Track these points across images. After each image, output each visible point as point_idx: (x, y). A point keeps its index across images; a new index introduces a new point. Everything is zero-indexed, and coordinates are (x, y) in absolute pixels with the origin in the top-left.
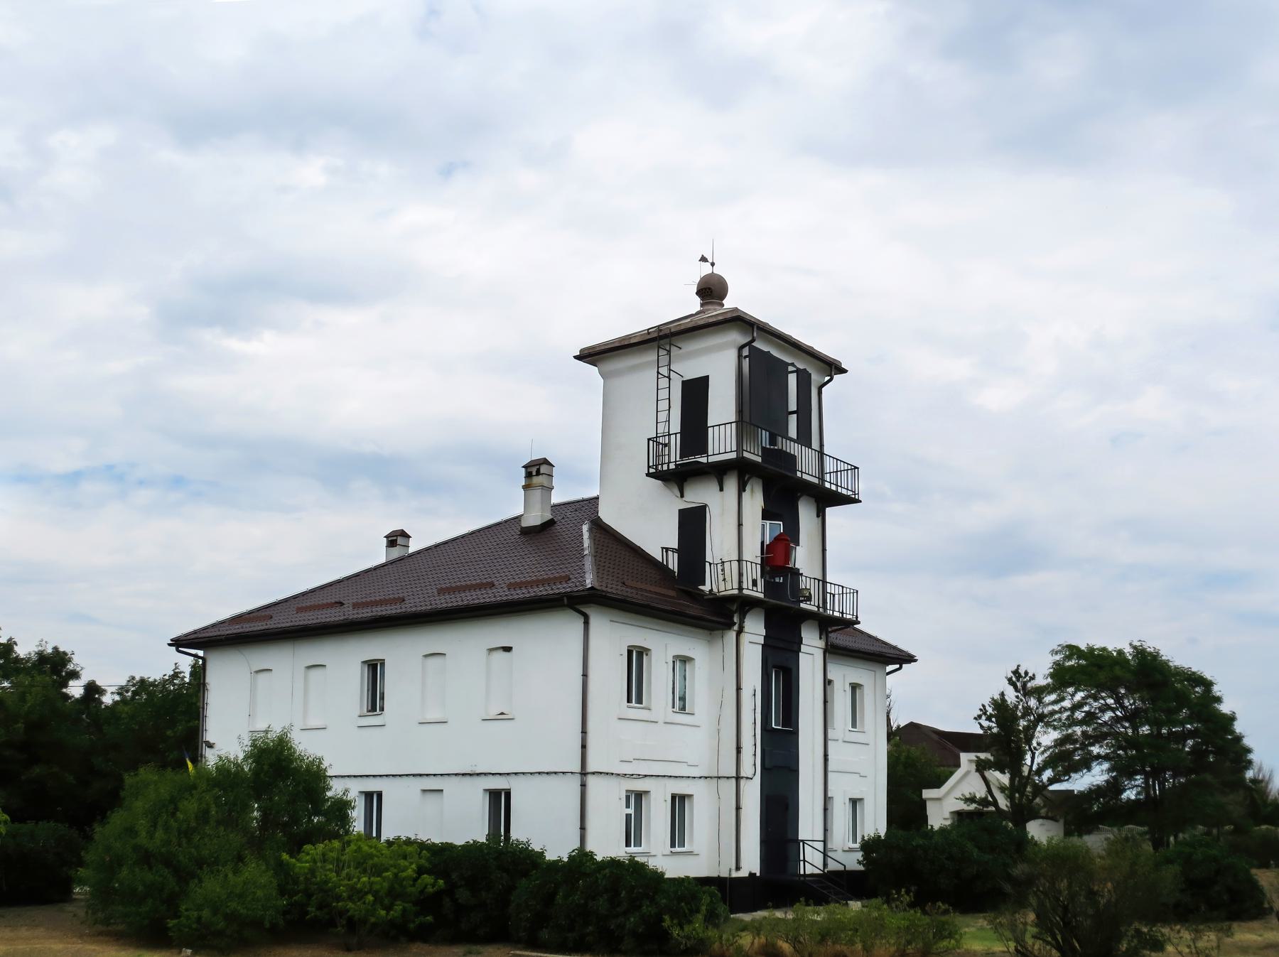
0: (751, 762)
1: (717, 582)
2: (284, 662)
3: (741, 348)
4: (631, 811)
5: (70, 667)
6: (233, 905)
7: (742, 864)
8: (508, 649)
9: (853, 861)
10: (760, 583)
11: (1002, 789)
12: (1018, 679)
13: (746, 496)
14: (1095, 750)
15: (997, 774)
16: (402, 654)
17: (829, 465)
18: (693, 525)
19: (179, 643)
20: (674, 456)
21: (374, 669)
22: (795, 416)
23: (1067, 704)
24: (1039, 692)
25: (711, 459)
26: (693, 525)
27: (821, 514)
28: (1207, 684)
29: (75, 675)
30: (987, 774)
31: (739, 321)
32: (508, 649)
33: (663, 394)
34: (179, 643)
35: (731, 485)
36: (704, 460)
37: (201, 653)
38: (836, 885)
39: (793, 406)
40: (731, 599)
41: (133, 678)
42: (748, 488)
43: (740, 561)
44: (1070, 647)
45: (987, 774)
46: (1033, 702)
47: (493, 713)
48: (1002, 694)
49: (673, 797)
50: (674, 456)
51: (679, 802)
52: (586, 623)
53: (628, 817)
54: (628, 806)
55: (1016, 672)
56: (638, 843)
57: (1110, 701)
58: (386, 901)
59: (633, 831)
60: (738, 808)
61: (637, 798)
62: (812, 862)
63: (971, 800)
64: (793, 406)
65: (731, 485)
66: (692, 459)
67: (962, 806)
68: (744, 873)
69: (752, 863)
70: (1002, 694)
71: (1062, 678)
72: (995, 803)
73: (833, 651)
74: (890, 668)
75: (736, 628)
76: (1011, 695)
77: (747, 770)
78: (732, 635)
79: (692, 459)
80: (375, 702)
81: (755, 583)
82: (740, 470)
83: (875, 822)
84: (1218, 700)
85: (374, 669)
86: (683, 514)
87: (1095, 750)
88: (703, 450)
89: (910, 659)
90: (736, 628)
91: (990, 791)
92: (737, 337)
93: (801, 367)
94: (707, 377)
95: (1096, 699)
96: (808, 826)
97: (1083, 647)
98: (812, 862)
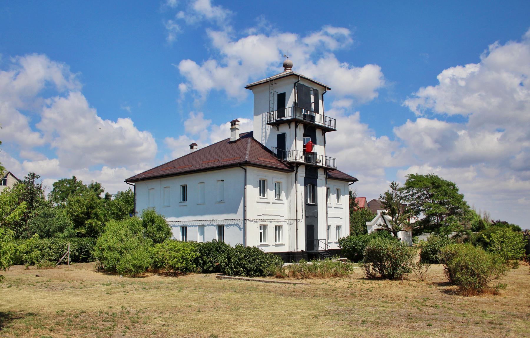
0: (301, 215)
1: (290, 158)
2: (157, 186)
3: (295, 84)
4: (262, 231)
5: (101, 188)
6: (135, 262)
7: (298, 247)
8: (223, 181)
9: (335, 246)
10: (303, 157)
11: (390, 221)
12: (393, 186)
13: (298, 130)
14: (421, 208)
15: (388, 216)
16: (191, 182)
17: (326, 119)
18: (281, 139)
19: (127, 181)
20: (275, 118)
21: (184, 188)
22: (313, 104)
23: (411, 193)
24: (401, 190)
25: (286, 119)
26: (281, 139)
27: (324, 134)
28: (454, 185)
29: (102, 191)
30: (385, 216)
31: (293, 75)
32: (223, 181)
33: (272, 98)
34: (127, 181)
35: (293, 125)
36: (284, 119)
37: (134, 184)
38: (331, 253)
39: (312, 101)
40: (293, 163)
41: (119, 192)
42: (298, 127)
43: (296, 151)
44: (411, 175)
45: (385, 216)
46: (398, 193)
47: (219, 200)
48: (388, 191)
49: (276, 227)
50: (275, 118)
51: (278, 228)
52: (246, 172)
53: (261, 233)
54: (261, 229)
55: (393, 184)
56: (279, 240)
57: (425, 192)
58: (181, 261)
59: (262, 237)
60: (297, 230)
61: (263, 228)
62: (322, 247)
63: (380, 225)
64: (312, 101)
65: (293, 125)
66: (280, 119)
67: (377, 227)
68: (299, 250)
69: (302, 247)
70: (388, 191)
71: (409, 185)
72: (387, 226)
73: (329, 177)
74: (350, 183)
75: (295, 172)
76: (391, 191)
77: (300, 217)
78: (294, 174)
79: (280, 119)
80: (184, 198)
81: (301, 157)
82: (295, 122)
83: (345, 233)
84: (457, 190)
85: (184, 188)
86: (279, 136)
87: (421, 208)
88: (284, 116)
89: (356, 180)
90: (295, 172)
91: (385, 222)
92: (294, 80)
93: (315, 88)
94: (284, 93)
95: (421, 192)
96: (321, 234)
97: (415, 175)
98: (322, 247)
